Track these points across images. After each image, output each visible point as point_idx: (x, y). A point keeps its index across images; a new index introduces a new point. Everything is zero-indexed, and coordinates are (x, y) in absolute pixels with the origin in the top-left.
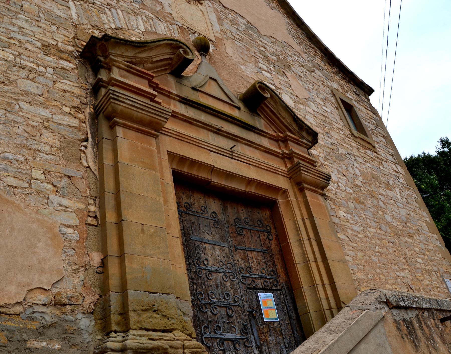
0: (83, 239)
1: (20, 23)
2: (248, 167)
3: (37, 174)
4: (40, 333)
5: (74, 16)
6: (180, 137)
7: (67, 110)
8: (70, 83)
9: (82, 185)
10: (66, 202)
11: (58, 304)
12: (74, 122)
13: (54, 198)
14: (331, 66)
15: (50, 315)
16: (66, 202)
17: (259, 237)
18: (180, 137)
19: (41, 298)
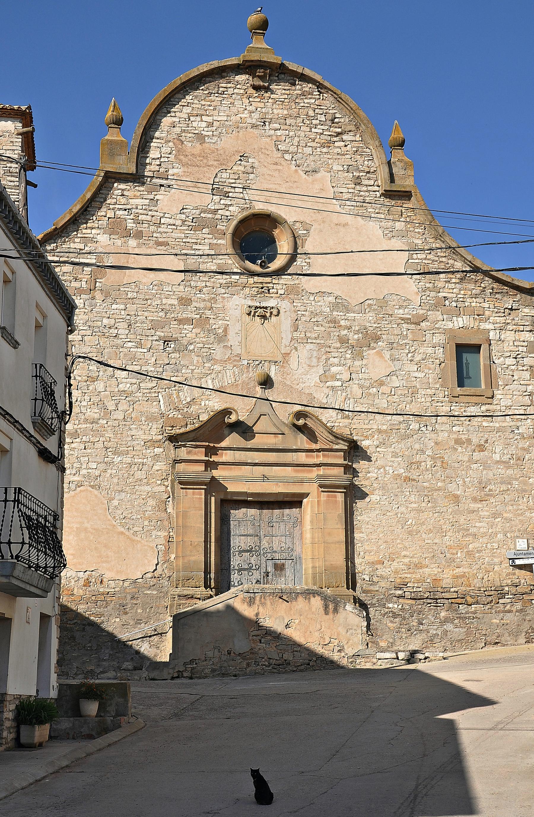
2: (347, 249)
12: (163, 488)
19: (149, 575)
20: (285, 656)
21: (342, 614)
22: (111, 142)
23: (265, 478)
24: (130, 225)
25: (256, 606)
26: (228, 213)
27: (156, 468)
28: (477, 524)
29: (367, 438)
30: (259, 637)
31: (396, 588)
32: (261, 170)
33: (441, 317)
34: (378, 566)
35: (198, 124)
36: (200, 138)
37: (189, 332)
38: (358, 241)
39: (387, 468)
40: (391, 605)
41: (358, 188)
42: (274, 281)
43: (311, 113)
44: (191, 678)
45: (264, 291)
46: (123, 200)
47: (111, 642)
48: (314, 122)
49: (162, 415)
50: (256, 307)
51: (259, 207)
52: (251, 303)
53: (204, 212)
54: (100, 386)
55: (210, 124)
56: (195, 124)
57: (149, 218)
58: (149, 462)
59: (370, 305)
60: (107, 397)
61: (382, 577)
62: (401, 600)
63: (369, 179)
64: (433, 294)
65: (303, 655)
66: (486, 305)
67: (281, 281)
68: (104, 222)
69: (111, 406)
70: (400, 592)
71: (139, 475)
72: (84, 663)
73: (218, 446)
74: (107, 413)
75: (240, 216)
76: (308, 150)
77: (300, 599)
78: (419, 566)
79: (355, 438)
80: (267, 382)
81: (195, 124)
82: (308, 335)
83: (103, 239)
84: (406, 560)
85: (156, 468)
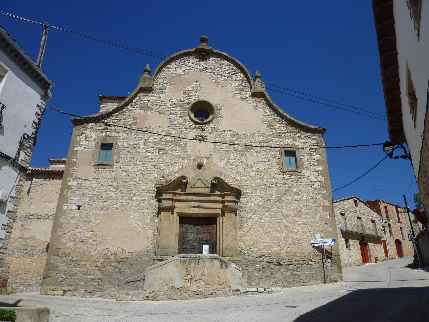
0: (154, 238)
1: (142, 187)
3: (145, 226)
4: (144, 256)
5: (156, 176)
6: (181, 207)
7: (152, 208)
8: (26, 308)
9: (154, 226)
10: (150, 231)
11: (148, 251)
12: (154, 211)
13: (148, 231)
14: (206, 59)
15: (146, 253)
16: (150, 231)
17: (191, 233)
18: (181, 207)
19: (144, 250)
20: (201, 290)
21: (230, 269)
22: (145, 77)
23: (198, 207)
24: (149, 106)
25: (186, 264)
26: (189, 101)
27: (151, 202)
28: (297, 228)
29: (246, 189)
30: (187, 280)
31: (260, 257)
32: (202, 86)
33: (278, 140)
34: (251, 247)
35: (179, 71)
36: (179, 75)
37: (170, 146)
38: (243, 113)
39: (255, 203)
40: (257, 265)
41: (242, 92)
42: (207, 126)
43: (224, 67)
44: (152, 300)
45: (202, 130)
46: (147, 97)
47: (14, 289)
48: (225, 70)
49: (156, 180)
50: (199, 136)
51: (202, 99)
52: (196, 135)
53: (179, 101)
54: (130, 168)
55: (183, 71)
56: (177, 71)
57: (157, 103)
58: (148, 199)
59: (247, 135)
60: (132, 172)
61: (253, 252)
62: (262, 263)
63: (247, 89)
64: (274, 131)
65: (209, 289)
66: (297, 135)
67: (210, 126)
68: (138, 105)
69: (134, 175)
70: (262, 259)
71: (144, 205)
72: (111, 291)
73: (175, 192)
74: (132, 178)
75: (193, 102)
76: (222, 79)
77: (208, 261)
78: (271, 247)
79: (241, 189)
80: (200, 166)
81: (177, 71)
82: (221, 147)
83: (137, 111)
84: (265, 244)
85: (151, 202)
